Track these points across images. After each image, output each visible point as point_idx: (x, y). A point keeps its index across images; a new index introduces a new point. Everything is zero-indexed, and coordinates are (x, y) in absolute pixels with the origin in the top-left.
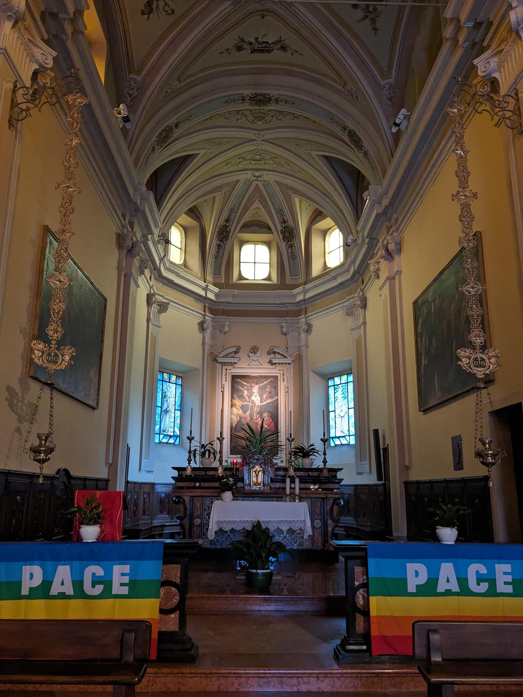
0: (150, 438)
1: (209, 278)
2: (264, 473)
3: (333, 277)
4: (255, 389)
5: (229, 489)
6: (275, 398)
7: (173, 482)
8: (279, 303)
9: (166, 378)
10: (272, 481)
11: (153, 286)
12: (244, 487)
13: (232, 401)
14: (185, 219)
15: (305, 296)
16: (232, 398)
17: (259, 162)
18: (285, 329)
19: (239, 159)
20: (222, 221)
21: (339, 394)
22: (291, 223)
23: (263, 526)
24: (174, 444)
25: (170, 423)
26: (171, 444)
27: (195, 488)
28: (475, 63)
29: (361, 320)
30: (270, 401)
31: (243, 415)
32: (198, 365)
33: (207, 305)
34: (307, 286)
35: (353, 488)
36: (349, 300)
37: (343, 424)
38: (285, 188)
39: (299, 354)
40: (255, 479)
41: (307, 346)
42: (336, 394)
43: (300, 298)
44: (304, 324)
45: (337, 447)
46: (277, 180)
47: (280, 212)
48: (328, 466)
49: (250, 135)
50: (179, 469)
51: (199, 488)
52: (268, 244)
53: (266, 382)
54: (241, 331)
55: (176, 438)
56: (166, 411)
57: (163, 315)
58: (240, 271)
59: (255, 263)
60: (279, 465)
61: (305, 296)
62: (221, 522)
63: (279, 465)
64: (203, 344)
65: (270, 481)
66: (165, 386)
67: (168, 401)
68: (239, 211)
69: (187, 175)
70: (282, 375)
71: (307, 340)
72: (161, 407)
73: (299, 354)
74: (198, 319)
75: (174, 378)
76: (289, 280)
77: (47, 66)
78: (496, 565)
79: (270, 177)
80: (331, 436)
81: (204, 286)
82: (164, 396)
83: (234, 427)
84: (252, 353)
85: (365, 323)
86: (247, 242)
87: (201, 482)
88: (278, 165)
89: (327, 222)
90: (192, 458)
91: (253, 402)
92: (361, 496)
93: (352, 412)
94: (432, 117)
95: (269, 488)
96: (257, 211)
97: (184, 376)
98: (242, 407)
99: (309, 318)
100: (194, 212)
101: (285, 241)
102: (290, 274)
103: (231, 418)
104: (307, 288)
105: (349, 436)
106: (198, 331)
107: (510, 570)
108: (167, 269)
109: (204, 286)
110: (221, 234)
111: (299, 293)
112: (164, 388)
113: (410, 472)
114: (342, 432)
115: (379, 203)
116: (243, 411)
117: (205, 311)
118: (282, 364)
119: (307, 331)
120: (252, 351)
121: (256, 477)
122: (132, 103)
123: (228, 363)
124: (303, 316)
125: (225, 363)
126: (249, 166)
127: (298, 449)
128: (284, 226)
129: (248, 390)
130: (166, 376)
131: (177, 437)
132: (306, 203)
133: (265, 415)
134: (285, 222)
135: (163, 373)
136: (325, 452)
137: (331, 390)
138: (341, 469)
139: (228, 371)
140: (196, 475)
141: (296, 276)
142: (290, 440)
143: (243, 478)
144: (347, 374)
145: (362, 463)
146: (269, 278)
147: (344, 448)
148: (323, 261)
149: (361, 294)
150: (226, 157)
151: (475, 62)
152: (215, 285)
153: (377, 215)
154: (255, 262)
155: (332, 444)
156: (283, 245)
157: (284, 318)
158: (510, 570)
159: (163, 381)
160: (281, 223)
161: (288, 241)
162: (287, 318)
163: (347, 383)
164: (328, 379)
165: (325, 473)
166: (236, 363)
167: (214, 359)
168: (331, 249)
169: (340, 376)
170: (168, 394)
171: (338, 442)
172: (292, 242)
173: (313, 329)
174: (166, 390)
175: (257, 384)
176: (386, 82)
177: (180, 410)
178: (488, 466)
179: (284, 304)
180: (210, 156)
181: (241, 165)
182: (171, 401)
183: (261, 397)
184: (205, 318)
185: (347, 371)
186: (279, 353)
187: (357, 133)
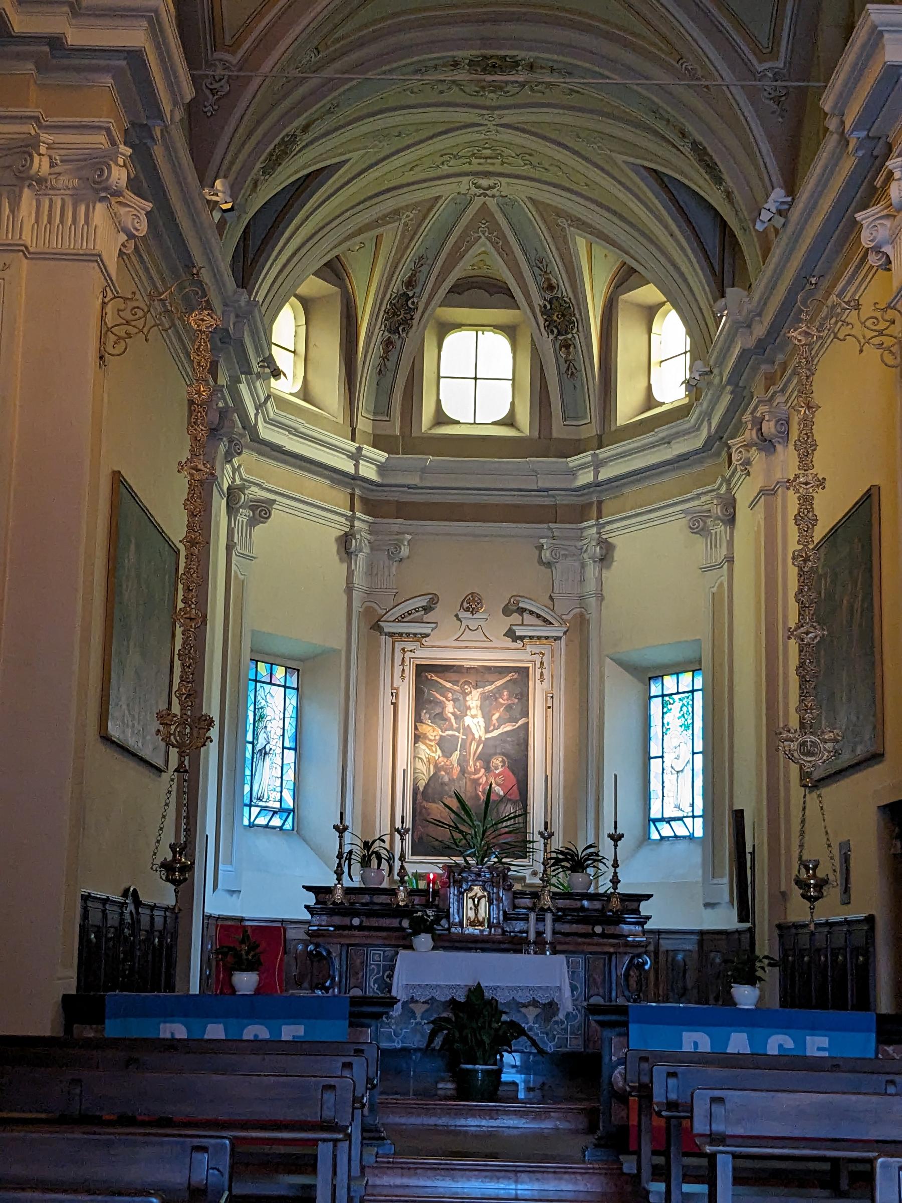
0: (235, 815)
1: (364, 424)
2: (490, 902)
3: (663, 439)
4: (474, 699)
5: (429, 929)
6: (520, 722)
7: (308, 916)
8: (535, 488)
9: (264, 673)
10: (507, 917)
11: (240, 466)
12: (449, 929)
13: (416, 728)
14: (312, 285)
15: (596, 474)
16: (418, 719)
17: (489, 161)
18: (548, 553)
19: (442, 156)
20: (397, 286)
21: (673, 717)
22: (565, 289)
23: (486, 994)
24: (281, 828)
25: (271, 779)
26: (274, 828)
27: (351, 927)
28: (858, 219)
29: (724, 551)
30: (508, 727)
31: (442, 761)
32: (338, 643)
33: (357, 492)
34: (603, 453)
35: (695, 938)
36: (699, 496)
37: (678, 791)
38: (552, 216)
39: (582, 615)
40: (471, 914)
41: (601, 597)
42: (665, 716)
43: (585, 478)
44: (594, 543)
45: (666, 843)
46: (534, 197)
47: (540, 265)
48: (621, 889)
49: (470, 116)
50: (316, 890)
51: (360, 928)
52: (510, 331)
53: (499, 683)
54: (438, 555)
55: (285, 815)
56: (264, 753)
57: (258, 529)
58: (438, 402)
59: (476, 379)
60: (528, 881)
61: (596, 474)
62: (414, 987)
63: (528, 881)
64: (349, 590)
65: (501, 918)
66: (261, 693)
67: (269, 729)
68: (439, 263)
69: (321, 200)
70: (538, 665)
71: (600, 581)
72: (252, 743)
73: (582, 615)
74: (338, 527)
75: (279, 672)
76: (559, 430)
77: (137, 234)
78: (808, 1037)
79: (519, 191)
80: (652, 816)
81: (353, 450)
82: (259, 718)
83: (421, 789)
84: (467, 610)
85: (730, 560)
86: (458, 326)
87: (368, 914)
88: (534, 167)
89: (649, 293)
90: (346, 869)
91: (467, 730)
92: (712, 955)
93: (699, 759)
94: (844, 191)
95: (500, 931)
96: (482, 257)
97: (304, 669)
98: (441, 742)
99: (607, 528)
100: (334, 270)
101: (552, 332)
102: (564, 412)
103: (415, 769)
104: (601, 456)
105: (693, 817)
106: (337, 558)
107: (826, 1045)
108: (269, 421)
109: (353, 450)
110: (395, 314)
111: (583, 467)
112: (259, 698)
113: (788, 905)
114: (678, 807)
115: (749, 326)
116: (443, 751)
117: (352, 509)
118: (539, 638)
119: (601, 560)
120: (465, 605)
121: (474, 909)
122: (216, 107)
123: (408, 635)
124: (593, 522)
125: (401, 635)
126: (466, 168)
127: (562, 853)
128: (548, 297)
129: (454, 700)
130: (262, 668)
131: (288, 811)
132: (599, 250)
133: (497, 761)
134: (551, 288)
135: (257, 661)
136: (616, 860)
137: (656, 706)
138: (648, 897)
139: (408, 655)
140: (352, 904)
141: (576, 418)
142: (547, 836)
143: (448, 910)
144: (693, 671)
145: (715, 881)
146: (509, 421)
147: (681, 846)
148: (645, 384)
149: (723, 490)
150: (406, 160)
151: (859, 216)
152: (378, 442)
153: (744, 352)
154: (477, 375)
155: (655, 836)
156: (547, 343)
157: (546, 526)
158: (826, 1045)
159: (256, 681)
160: (541, 289)
161: (559, 334)
162: (552, 525)
163: (692, 691)
164: (650, 679)
165: (615, 903)
166: (427, 635)
167: (375, 625)
168: (661, 359)
169: (678, 674)
170: (268, 711)
171: (666, 830)
172: (570, 336)
173: (617, 554)
174: (264, 703)
175: (476, 687)
176: (767, 65)
177: (295, 749)
178: (810, 901)
179: (547, 490)
180: (373, 160)
181: (446, 167)
182: (274, 727)
183: (487, 717)
184: (352, 526)
185: (691, 662)
186: (531, 613)
187: (709, 150)
